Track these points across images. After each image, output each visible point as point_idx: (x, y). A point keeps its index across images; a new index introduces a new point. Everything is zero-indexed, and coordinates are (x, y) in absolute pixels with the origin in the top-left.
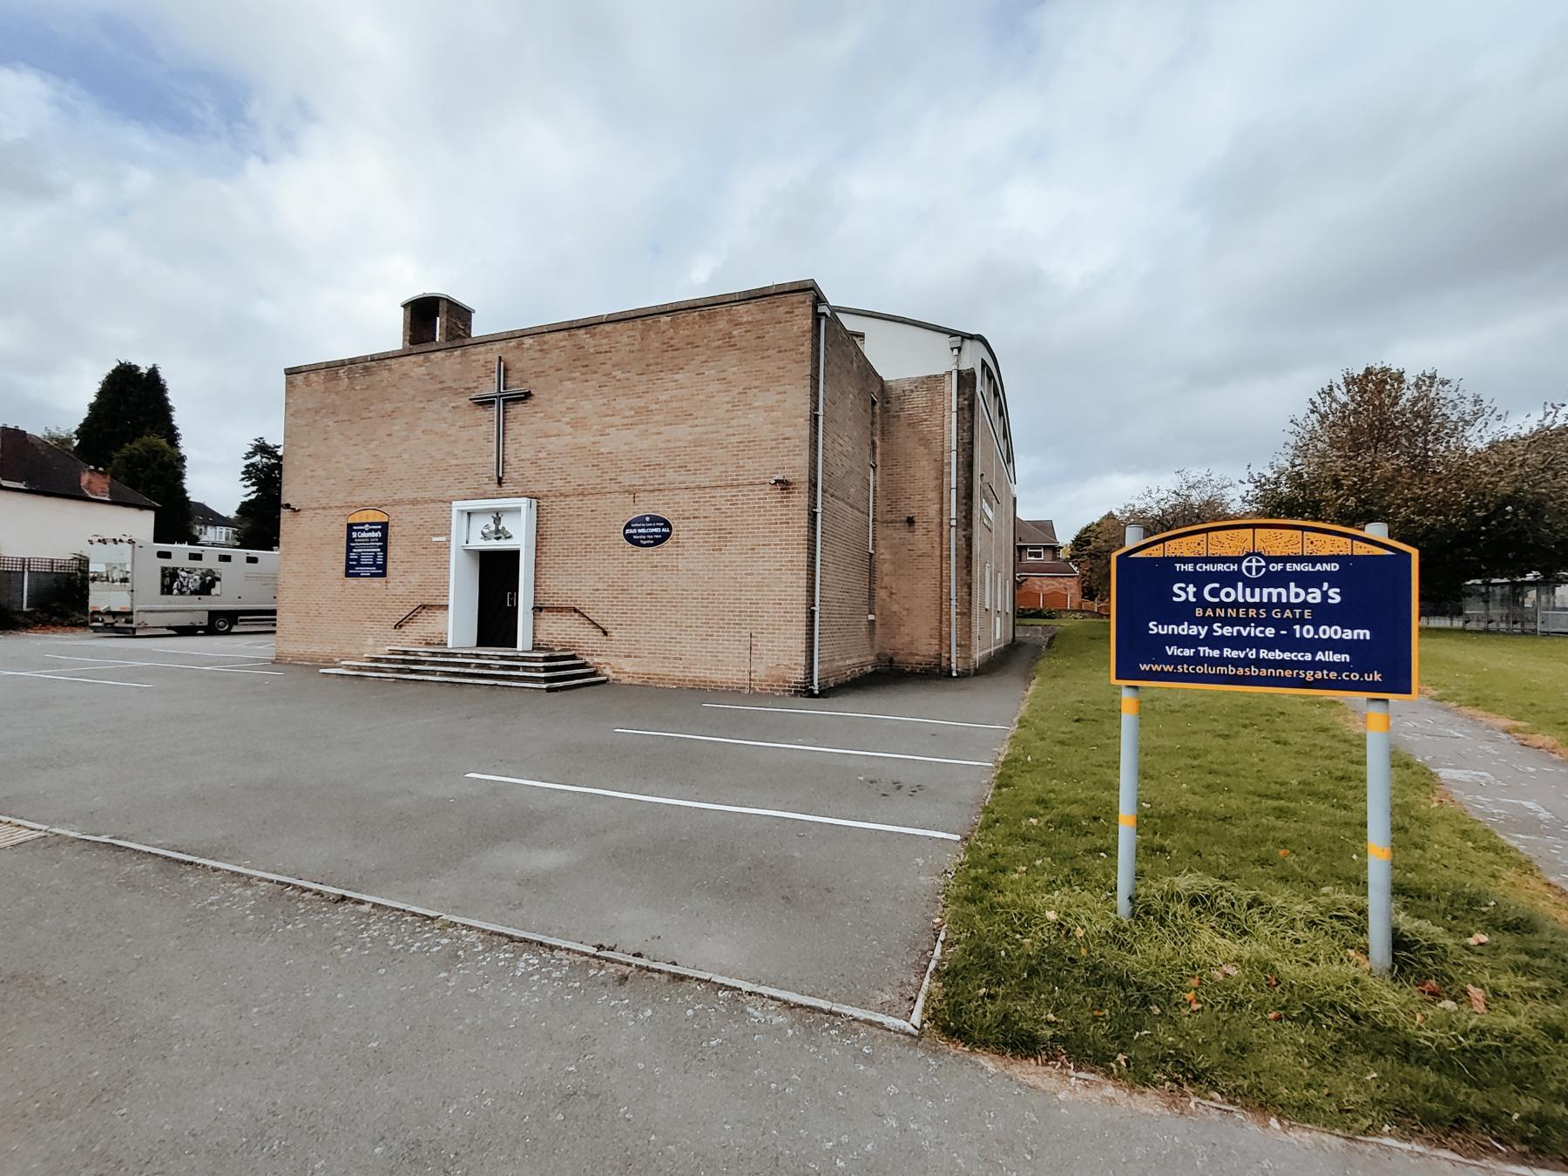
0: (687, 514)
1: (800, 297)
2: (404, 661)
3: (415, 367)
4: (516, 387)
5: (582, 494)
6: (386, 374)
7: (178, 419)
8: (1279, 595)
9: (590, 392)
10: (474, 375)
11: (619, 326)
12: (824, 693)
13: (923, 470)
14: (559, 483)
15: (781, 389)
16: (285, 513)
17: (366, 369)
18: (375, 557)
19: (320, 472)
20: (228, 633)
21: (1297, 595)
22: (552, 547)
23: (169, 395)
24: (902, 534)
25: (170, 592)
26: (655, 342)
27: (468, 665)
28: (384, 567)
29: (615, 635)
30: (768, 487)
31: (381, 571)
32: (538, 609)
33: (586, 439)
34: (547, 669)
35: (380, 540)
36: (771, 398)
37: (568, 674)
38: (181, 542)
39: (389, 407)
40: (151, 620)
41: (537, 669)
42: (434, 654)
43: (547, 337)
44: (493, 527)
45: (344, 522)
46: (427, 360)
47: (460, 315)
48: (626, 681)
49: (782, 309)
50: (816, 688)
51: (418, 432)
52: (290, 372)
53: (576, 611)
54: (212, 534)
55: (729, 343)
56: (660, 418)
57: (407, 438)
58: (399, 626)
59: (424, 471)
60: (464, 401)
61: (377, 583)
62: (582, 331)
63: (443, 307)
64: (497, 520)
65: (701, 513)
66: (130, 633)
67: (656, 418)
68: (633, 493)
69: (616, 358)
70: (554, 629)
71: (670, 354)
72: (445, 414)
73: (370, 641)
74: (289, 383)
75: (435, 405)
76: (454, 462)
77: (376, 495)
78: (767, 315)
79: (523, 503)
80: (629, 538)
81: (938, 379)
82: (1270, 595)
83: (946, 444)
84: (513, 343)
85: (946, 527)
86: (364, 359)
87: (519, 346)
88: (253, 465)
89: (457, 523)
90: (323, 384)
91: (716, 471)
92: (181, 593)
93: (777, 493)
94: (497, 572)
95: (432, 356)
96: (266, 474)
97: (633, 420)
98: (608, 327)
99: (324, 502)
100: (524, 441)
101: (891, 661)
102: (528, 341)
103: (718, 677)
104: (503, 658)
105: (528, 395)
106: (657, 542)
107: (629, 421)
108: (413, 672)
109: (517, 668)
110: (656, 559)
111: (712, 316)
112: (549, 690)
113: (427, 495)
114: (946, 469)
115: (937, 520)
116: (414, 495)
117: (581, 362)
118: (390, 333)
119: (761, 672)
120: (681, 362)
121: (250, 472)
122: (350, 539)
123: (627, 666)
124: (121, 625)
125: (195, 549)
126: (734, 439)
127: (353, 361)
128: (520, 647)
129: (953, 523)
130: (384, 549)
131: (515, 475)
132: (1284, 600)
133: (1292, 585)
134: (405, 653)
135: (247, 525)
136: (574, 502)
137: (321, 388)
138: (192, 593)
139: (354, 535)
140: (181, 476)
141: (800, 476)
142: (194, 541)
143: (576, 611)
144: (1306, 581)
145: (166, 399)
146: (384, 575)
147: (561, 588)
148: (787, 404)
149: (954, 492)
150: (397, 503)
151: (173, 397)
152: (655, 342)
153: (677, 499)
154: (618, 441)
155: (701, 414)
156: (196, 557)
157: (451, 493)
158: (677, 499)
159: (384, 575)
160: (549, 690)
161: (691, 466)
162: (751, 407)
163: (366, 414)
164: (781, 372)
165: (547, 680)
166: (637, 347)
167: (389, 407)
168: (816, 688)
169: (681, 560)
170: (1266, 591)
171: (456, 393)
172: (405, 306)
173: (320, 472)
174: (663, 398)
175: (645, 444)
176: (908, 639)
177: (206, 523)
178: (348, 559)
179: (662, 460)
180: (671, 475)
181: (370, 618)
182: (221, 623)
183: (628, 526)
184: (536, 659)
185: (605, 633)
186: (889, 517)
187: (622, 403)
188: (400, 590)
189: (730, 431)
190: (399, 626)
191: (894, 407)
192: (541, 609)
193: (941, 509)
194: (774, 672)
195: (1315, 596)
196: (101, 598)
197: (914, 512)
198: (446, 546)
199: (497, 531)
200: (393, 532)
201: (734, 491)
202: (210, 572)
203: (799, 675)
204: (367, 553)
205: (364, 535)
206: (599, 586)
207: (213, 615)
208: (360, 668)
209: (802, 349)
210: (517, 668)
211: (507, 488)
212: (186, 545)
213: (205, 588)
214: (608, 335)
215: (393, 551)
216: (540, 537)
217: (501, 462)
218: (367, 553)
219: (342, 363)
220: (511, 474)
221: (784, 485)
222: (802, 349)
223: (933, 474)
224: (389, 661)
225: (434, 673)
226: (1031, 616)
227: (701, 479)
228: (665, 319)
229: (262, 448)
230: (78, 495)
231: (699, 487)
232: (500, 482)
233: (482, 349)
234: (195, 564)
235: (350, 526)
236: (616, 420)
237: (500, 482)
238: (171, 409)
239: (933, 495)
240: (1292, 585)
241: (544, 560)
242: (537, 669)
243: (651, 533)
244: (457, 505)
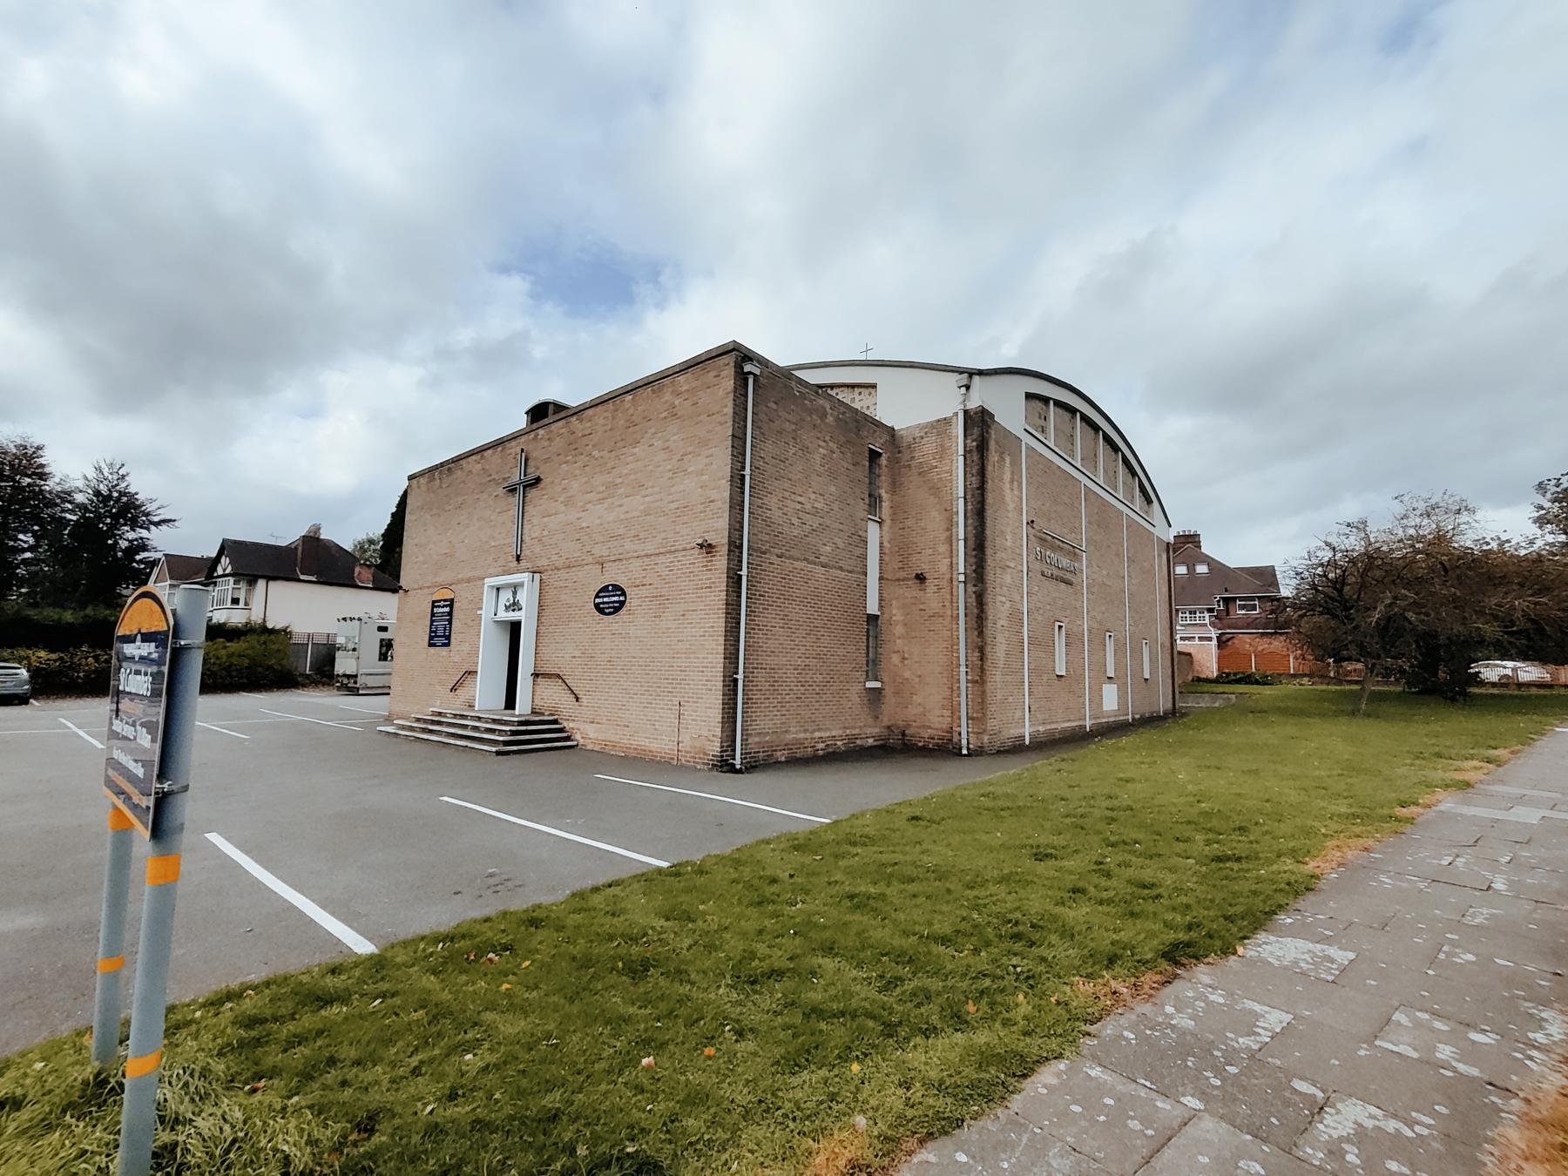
12: (751, 767)
13: (933, 520)
14: (554, 558)
24: (912, 591)
25: (385, 659)
28: (448, 638)
29: (584, 700)
30: (697, 551)
32: (536, 675)
40: (371, 681)
48: (590, 747)
50: (738, 762)
53: (559, 676)
60: (500, 491)
66: (354, 691)
75: (485, 495)
81: (946, 422)
89: (488, 597)
93: (698, 556)
98: (590, 412)
101: (904, 734)
103: (654, 746)
105: (538, 480)
108: (431, 732)
111: (661, 389)
112: (498, 753)
119: (686, 744)
124: (350, 686)
126: (675, 505)
128: (517, 712)
129: (962, 578)
141: (720, 538)
146: (448, 645)
149: (962, 543)
150: (460, 582)
159: (448, 645)
160: (498, 753)
162: (131, 541)
167: (460, 499)
168: (738, 762)
179: (621, 531)
180: (628, 546)
184: (506, 723)
186: (901, 574)
191: (905, 457)
194: (697, 744)
196: (344, 665)
197: (924, 568)
201: (671, 557)
203: (715, 748)
211: (523, 563)
221: (707, 547)
223: (944, 525)
226: (1238, 681)
228: (629, 397)
230: (351, 584)
232: (518, 558)
233: (513, 443)
237: (518, 558)
239: (943, 548)
243: (611, 601)
244: (490, 581)
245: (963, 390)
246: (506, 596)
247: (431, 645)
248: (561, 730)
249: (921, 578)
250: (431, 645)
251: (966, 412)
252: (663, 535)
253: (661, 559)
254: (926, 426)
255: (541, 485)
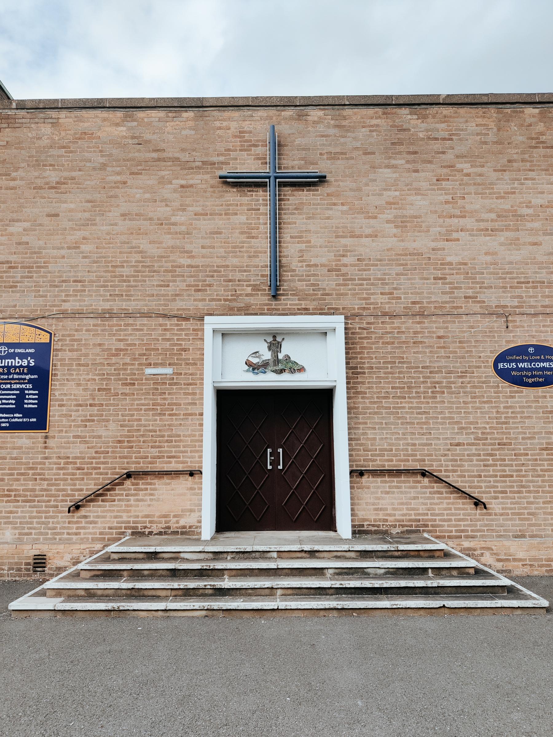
8: (12, 362)
9: (424, 185)
11: (463, 111)
18: (21, 397)
21: (19, 362)
22: (369, 383)
29: (495, 506)
32: (357, 473)
33: (421, 243)
43: (348, 112)
56: (536, 225)
57: (90, 222)
59: (126, 271)
60: (203, 180)
61: (25, 439)
67: (529, 225)
68: (504, 315)
69: (460, 149)
70: (387, 502)
76: (186, 261)
77: (29, 303)
80: (504, 374)
82: (8, 362)
97: (496, 225)
105: (322, 179)
107: (489, 225)
113: (132, 306)
116: (107, 306)
123: (520, 549)
132: (13, 365)
133: (17, 358)
136: (409, 324)
143: (424, 474)
144: (22, 356)
166: (491, 137)
170: (7, 361)
175: (516, 256)
185: (477, 503)
192: (361, 474)
195: (25, 363)
214: (445, 119)
215: (57, 390)
216: (353, 371)
217: (277, 267)
236: (469, 222)
240: (17, 358)
244: (212, 323)
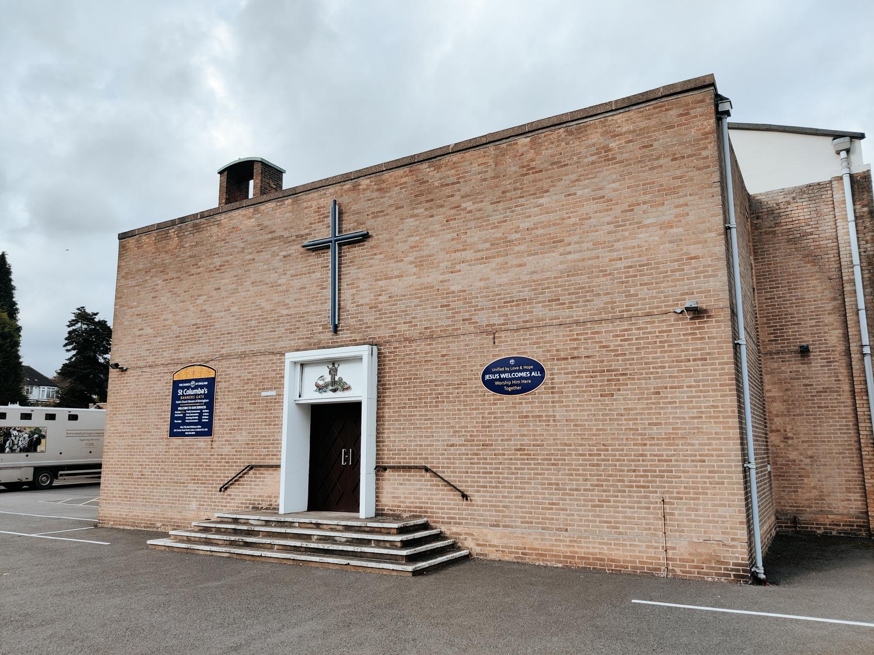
0: (562, 355)
1: (697, 95)
2: (236, 532)
3: (241, 219)
4: (350, 228)
5: (431, 337)
6: (215, 229)
7: (18, 297)
9: (437, 227)
10: (306, 222)
11: (467, 155)
13: (815, 292)
15: (682, 201)
16: (113, 373)
17: (195, 226)
18: (201, 415)
19: (148, 331)
20: (50, 487)
23: (12, 277)
24: (794, 365)
26: (511, 167)
27: (308, 537)
29: (477, 498)
30: (672, 318)
31: (206, 429)
32: (380, 469)
33: (433, 277)
34: (405, 544)
35: (206, 396)
36: (668, 213)
37: (428, 550)
38: (13, 402)
39: (217, 261)
41: (393, 545)
42: (267, 523)
43: (386, 175)
44: (328, 379)
45: (169, 379)
46: (256, 211)
47: (272, 174)
49: (674, 112)
51: (248, 283)
52: (122, 237)
53: (427, 470)
54: (37, 393)
55: (606, 156)
56: (522, 247)
57: (235, 291)
58: (224, 488)
59: (253, 323)
60: (295, 249)
62: (425, 165)
63: (257, 169)
64: (333, 372)
65: (583, 352)
67: (517, 249)
68: (493, 333)
69: (466, 189)
71: (531, 177)
72: (276, 263)
73: (194, 505)
74: (122, 248)
75: (266, 255)
78: (653, 122)
79: (364, 350)
80: (489, 384)
81: (820, 187)
83: (844, 260)
84: (348, 185)
85: (855, 356)
86: (194, 216)
87: (355, 188)
88: (74, 330)
90: (154, 248)
91: (599, 302)
92: (12, 450)
93: (686, 325)
94: (333, 428)
95: (262, 207)
96: (90, 338)
98: (455, 158)
99: (150, 360)
100: (362, 285)
101: (795, 521)
102: (364, 182)
104: (348, 528)
105: (366, 237)
106: (526, 389)
108: (247, 545)
109: (367, 542)
110: (526, 408)
113: (256, 347)
114: (848, 288)
115: (841, 348)
117: (424, 195)
118: (209, 196)
120: (546, 184)
121: (72, 338)
122: (175, 397)
125: (26, 409)
126: (619, 264)
127: (183, 220)
130: (210, 406)
131: (352, 322)
134: (236, 521)
135: (67, 384)
137: (151, 249)
138: (21, 451)
139: (180, 392)
140: (17, 344)
142: (24, 402)
143: (427, 470)
145: (10, 280)
146: (209, 433)
147: (403, 443)
148: (692, 218)
149: (863, 314)
150: (223, 357)
151: (16, 278)
152: (511, 167)
153: (548, 337)
154: (471, 277)
155: (576, 238)
156: (26, 416)
157: (281, 344)
158: (548, 337)
159: (209, 433)
161: (565, 299)
162: (640, 225)
163: (193, 271)
164: (678, 182)
165: (411, 559)
166: (490, 174)
167: (217, 261)
169: (557, 410)
171: (287, 241)
172: (221, 173)
173: (148, 331)
174: (524, 225)
175: (504, 279)
176: (815, 493)
177: (33, 384)
178: (173, 418)
179: (526, 293)
180: (539, 311)
181: (195, 479)
182: (44, 479)
183: (487, 371)
185: (465, 496)
186: (773, 347)
187: (475, 236)
188: (226, 450)
189: (615, 255)
190: (224, 488)
191: (767, 223)
192: (385, 469)
193: (846, 337)
197: (807, 340)
198: (277, 401)
199: (333, 382)
200: (219, 387)
201: (625, 325)
202: (37, 430)
204: (193, 411)
205: (190, 392)
206: (455, 440)
207: (38, 470)
208: (189, 540)
209: (704, 153)
210: (367, 542)
211: (344, 335)
212: (17, 406)
213: (32, 446)
215: (220, 408)
217: (337, 308)
218: (193, 411)
219: (173, 223)
220: (348, 320)
221: (697, 313)
222: (704, 153)
224: (219, 531)
225: (271, 547)
227: (579, 313)
228: (524, 140)
229: (82, 316)
231: (577, 323)
232: (336, 330)
234: (26, 423)
235: (176, 384)
236: (469, 255)
237: (336, 330)
238: (13, 288)
239: (832, 319)
241: (388, 412)
242: (393, 545)
243: (514, 378)
245: (843, 154)
246: (314, 375)
247: (172, 434)
248: (439, 537)
249: (804, 351)
250: (172, 434)
251: (852, 177)
252: (607, 299)
253: (604, 327)
254: (793, 190)
255: (368, 244)
